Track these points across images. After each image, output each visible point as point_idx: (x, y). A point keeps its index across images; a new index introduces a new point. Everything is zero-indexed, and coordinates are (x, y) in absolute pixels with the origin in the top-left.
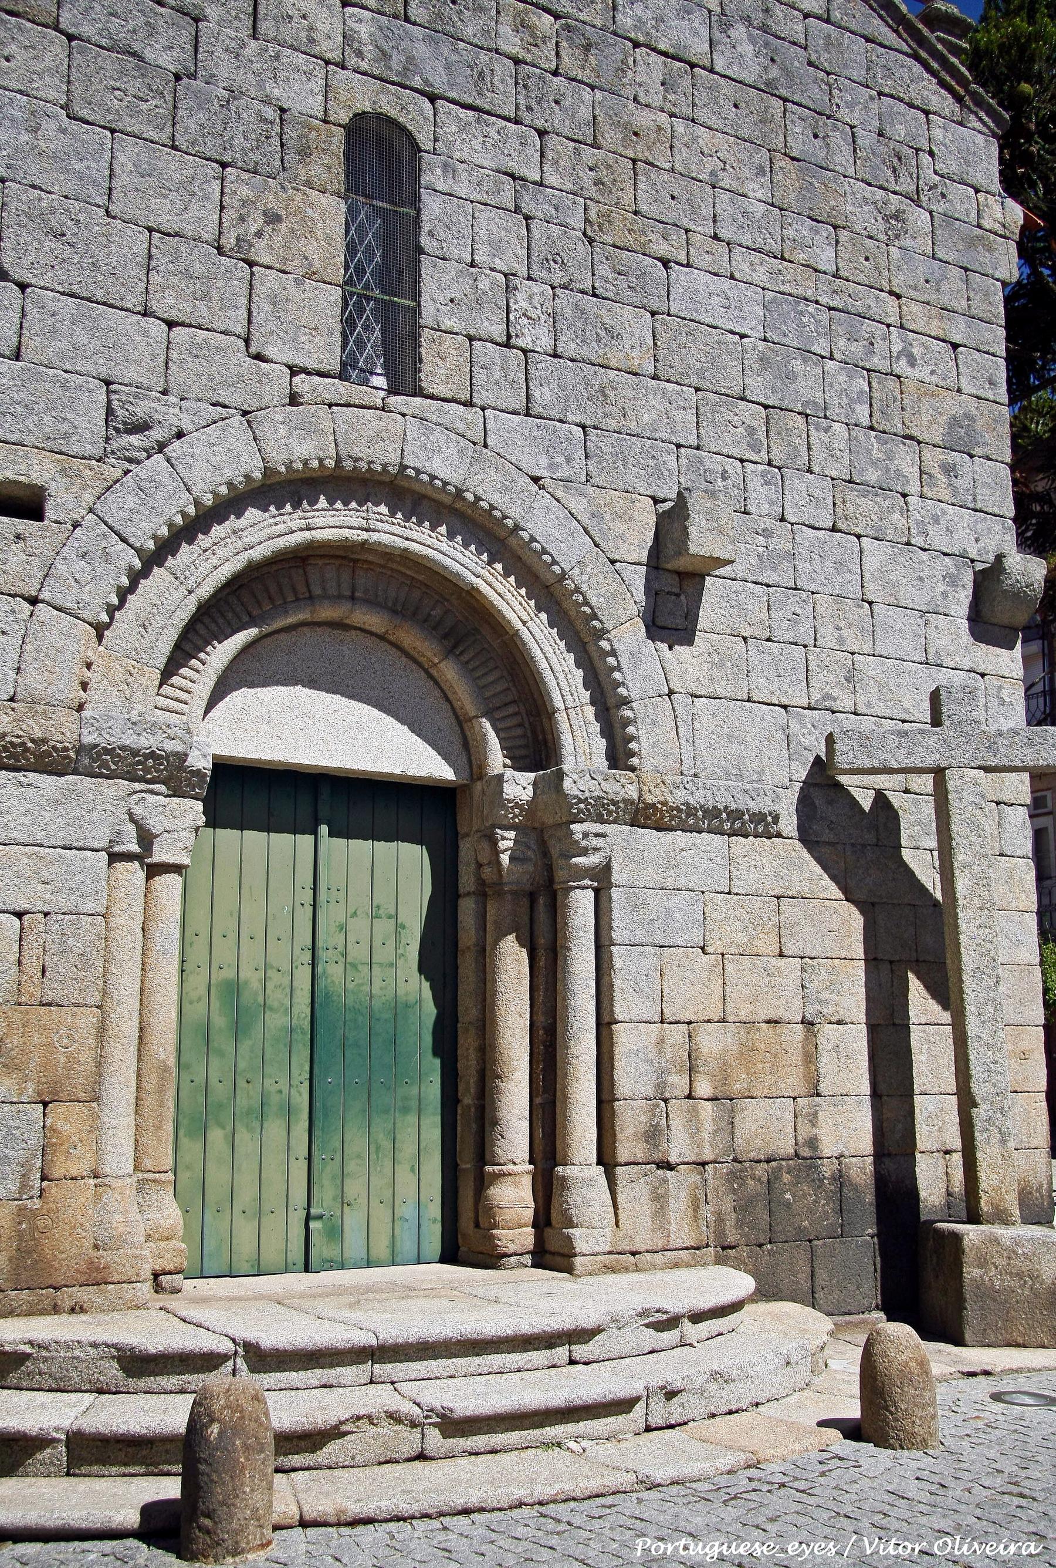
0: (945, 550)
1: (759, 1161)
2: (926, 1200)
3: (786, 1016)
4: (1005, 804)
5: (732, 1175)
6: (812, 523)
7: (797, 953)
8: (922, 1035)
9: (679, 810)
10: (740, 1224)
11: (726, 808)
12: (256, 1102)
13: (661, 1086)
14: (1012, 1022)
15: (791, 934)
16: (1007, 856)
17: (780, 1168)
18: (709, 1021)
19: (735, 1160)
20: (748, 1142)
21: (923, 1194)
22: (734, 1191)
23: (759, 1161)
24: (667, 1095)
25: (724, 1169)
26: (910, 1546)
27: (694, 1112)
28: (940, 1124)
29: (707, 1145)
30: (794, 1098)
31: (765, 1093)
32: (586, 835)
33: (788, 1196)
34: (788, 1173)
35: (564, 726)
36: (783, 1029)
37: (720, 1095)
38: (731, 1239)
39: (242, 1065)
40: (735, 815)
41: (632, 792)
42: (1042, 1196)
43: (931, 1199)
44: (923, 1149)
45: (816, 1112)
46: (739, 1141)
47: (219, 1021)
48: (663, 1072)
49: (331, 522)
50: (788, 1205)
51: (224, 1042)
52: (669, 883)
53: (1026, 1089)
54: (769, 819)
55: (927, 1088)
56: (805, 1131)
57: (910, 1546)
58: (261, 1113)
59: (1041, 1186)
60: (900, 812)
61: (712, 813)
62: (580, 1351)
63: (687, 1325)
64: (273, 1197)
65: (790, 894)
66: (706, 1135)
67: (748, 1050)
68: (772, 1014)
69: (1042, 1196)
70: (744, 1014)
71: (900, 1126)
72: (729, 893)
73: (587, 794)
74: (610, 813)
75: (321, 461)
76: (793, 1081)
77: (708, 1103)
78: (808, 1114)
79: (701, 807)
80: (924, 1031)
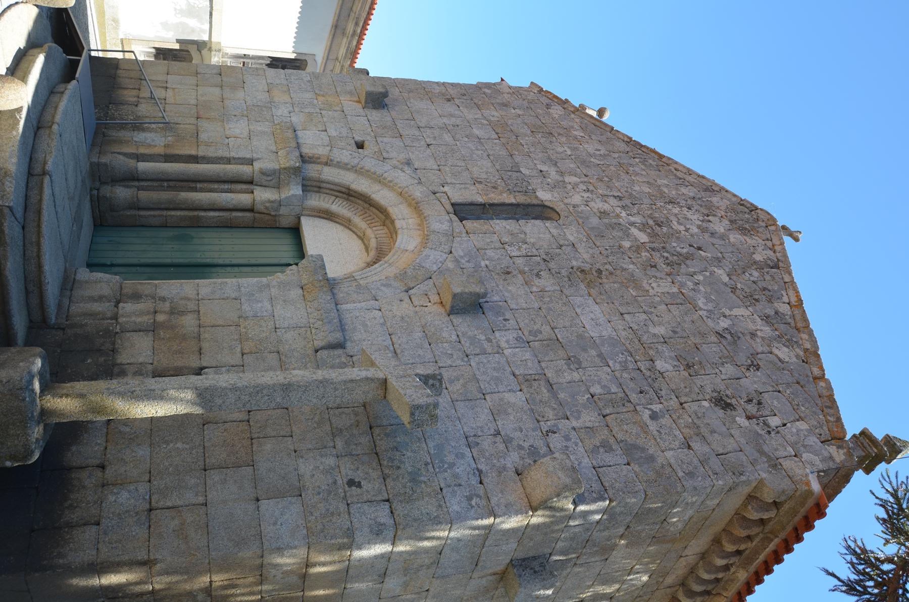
13: (163, 299)
45: (142, 375)
46: (128, 334)
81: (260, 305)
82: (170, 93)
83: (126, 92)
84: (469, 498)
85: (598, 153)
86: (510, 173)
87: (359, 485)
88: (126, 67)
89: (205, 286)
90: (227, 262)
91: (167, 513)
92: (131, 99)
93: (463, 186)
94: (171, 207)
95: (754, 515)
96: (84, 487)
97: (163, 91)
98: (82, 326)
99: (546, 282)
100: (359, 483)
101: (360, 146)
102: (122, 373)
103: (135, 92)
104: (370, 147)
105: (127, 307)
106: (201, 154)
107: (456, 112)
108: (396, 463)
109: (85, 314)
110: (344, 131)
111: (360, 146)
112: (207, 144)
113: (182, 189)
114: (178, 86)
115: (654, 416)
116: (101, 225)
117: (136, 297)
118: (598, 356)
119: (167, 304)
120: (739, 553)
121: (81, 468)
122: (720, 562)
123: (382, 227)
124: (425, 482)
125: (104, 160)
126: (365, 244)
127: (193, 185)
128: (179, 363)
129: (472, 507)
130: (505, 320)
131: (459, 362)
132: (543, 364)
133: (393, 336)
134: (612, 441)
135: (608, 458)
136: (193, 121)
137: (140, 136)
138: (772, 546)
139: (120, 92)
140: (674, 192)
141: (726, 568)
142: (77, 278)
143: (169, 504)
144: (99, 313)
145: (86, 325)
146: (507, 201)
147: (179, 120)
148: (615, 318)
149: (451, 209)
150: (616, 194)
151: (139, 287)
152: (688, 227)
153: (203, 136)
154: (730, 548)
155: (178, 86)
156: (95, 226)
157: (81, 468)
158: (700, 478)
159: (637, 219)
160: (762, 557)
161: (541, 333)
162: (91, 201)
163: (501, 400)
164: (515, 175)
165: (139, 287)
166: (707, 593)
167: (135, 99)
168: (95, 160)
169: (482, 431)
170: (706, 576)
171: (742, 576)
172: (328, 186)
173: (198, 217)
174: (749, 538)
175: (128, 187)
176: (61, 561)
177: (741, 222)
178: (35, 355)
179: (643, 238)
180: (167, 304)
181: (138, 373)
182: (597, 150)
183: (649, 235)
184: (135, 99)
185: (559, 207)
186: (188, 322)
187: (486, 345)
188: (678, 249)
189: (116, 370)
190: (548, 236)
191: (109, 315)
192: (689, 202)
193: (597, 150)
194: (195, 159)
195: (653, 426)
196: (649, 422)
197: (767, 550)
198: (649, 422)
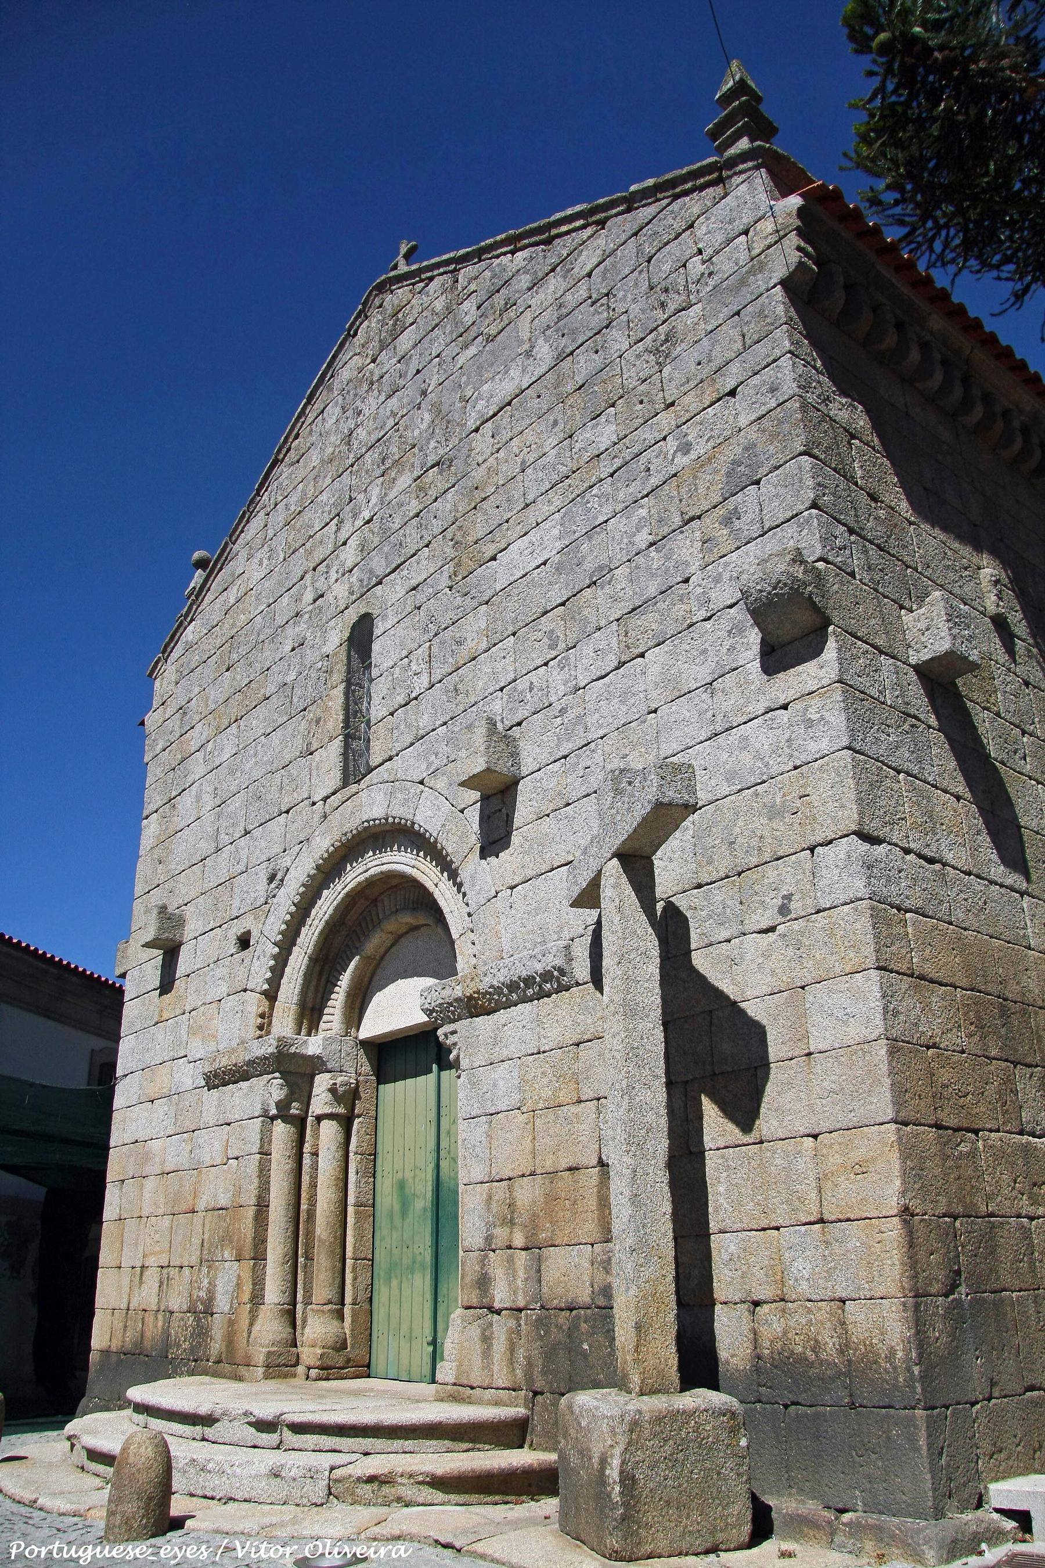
0: (729, 603)
1: (561, 1310)
2: (727, 1362)
3: (585, 1162)
4: (821, 845)
5: (539, 1322)
6: (599, 674)
7: (592, 1095)
8: (720, 1161)
9: (490, 993)
10: (544, 1373)
11: (519, 977)
12: (410, 1262)
13: (489, 1239)
14: (838, 1126)
15: (587, 1078)
16: (825, 910)
17: (578, 1317)
18: (523, 1176)
19: (542, 1307)
20: (550, 1288)
21: (723, 1354)
22: (541, 1338)
23: (561, 1310)
24: (493, 1247)
25: (534, 1315)
26: (36, 1550)
27: (511, 1261)
28: (744, 1268)
29: (520, 1293)
30: (592, 1245)
31: (566, 1240)
32: (446, 1035)
33: (586, 1346)
34: (585, 1322)
35: (296, 998)
36: (580, 1175)
37: (530, 1245)
38: (538, 1385)
39: (405, 1236)
40: (529, 981)
41: (458, 992)
42: (895, 1368)
43: (734, 1360)
44: (723, 1299)
45: (610, 1258)
46: (545, 1290)
47: (397, 1207)
48: (490, 1225)
49: (354, 876)
50: (585, 1355)
51: (398, 1221)
52: (495, 1057)
53: (864, 1215)
54: (556, 973)
55: (728, 1224)
56: (600, 1277)
57: (36, 1550)
58: (411, 1270)
59: (892, 1352)
60: (688, 914)
61: (513, 986)
62: (209, 1432)
63: (287, 1434)
64: (417, 1332)
65: (586, 1037)
66: (519, 1282)
67: (552, 1198)
68: (571, 1162)
69: (895, 1368)
70: (549, 1165)
71: (696, 1272)
72: (539, 1053)
73: (433, 1004)
74: (453, 1013)
75: (333, 845)
76: (589, 1228)
77: (523, 1252)
78: (602, 1262)
79: (503, 984)
80: (723, 1157)
81: (501, 1083)
82: (151, 1261)
83: (148, 1334)
84: (809, 723)
85: (265, 562)
86: (295, 700)
87: (788, 897)
88: (108, 1337)
89: (469, 1171)
90: (431, 1157)
91: (827, 1194)
92: (160, 1324)
93: (314, 773)
94: (338, 1250)
95: (838, 299)
96: (785, 1333)
97: (148, 1273)
98: (530, 1365)
99: (474, 628)
100: (784, 897)
101: (244, 942)
102: (607, 1291)
103: (150, 1319)
104: (248, 923)
105: (500, 1296)
106: (253, 1201)
107: (194, 793)
108: (754, 842)
109: (511, 1361)
110: (221, 971)
111: (244, 942)
112: (238, 1191)
113: (310, 1234)
114: (141, 1248)
115: (685, 448)
116: (368, 1366)
117: (484, 1282)
118: (590, 539)
119: (498, 1231)
120: (899, 326)
121: (756, 1340)
122: (914, 355)
123: (379, 904)
124: (784, 795)
125: (260, 1358)
126: (407, 933)
127: (303, 1216)
128: (592, 1203)
129: (822, 718)
130: (531, 689)
131: (598, 757)
132: (603, 623)
133: (583, 1098)
134: (720, 511)
135: (750, 514)
136: (198, 1218)
137: (222, 1303)
138: (889, 274)
139: (147, 1344)
140: (333, 439)
141: (925, 347)
142: (453, 1381)
143: (813, 1195)
144: (510, 1340)
145: (528, 1358)
146: (341, 700)
147: (196, 1241)
148: (532, 516)
149: (354, 788)
150: (334, 528)
151: (468, 1280)
152: (388, 413)
153: (224, 1201)
154: (891, 340)
155: (141, 1248)
156: (369, 1377)
157: (756, 1340)
158: (780, 375)
159: (375, 492)
160: (906, 291)
161: (552, 631)
162: (327, 1379)
163: (657, 685)
164: (298, 692)
165: (468, 1280)
166: (965, 380)
167: (160, 1317)
168: (261, 1370)
169: (706, 711)
170: (938, 378)
171: (937, 322)
172: (310, 995)
173: (357, 1205)
174: (875, 309)
175: (304, 1321)
176: (900, 1354)
177: (384, 334)
178: (570, 1407)
179: (405, 481)
180: (498, 1231)
181: (606, 1265)
182: (261, 563)
183: (400, 472)
184: (160, 1317)
185: (352, 616)
186: (526, 1194)
187: (570, 715)
188: (424, 426)
189: (601, 1301)
190: (399, 631)
191: (512, 1323)
192: (350, 413)
193: (261, 563)
194: (262, 1206)
195: (700, 448)
196: (693, 455)
197: (894, 281)
198: (693, 455)
